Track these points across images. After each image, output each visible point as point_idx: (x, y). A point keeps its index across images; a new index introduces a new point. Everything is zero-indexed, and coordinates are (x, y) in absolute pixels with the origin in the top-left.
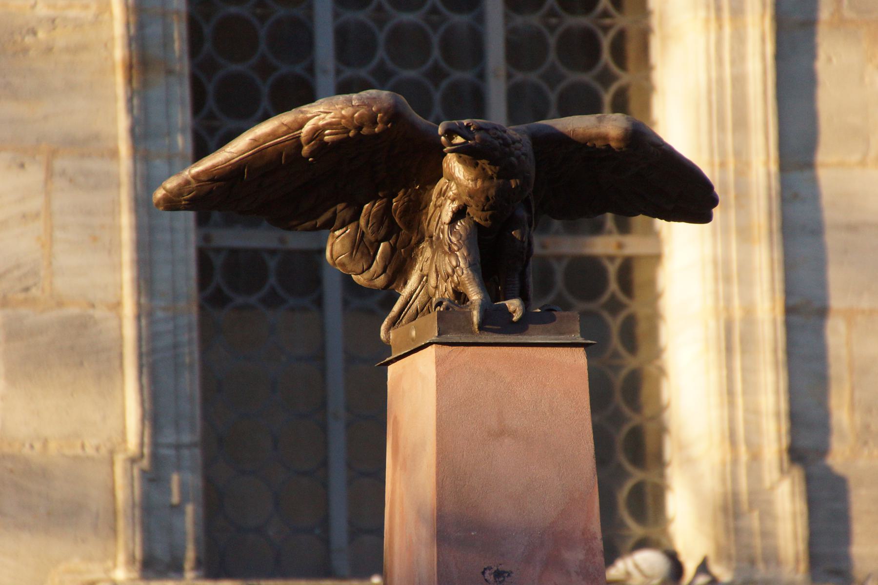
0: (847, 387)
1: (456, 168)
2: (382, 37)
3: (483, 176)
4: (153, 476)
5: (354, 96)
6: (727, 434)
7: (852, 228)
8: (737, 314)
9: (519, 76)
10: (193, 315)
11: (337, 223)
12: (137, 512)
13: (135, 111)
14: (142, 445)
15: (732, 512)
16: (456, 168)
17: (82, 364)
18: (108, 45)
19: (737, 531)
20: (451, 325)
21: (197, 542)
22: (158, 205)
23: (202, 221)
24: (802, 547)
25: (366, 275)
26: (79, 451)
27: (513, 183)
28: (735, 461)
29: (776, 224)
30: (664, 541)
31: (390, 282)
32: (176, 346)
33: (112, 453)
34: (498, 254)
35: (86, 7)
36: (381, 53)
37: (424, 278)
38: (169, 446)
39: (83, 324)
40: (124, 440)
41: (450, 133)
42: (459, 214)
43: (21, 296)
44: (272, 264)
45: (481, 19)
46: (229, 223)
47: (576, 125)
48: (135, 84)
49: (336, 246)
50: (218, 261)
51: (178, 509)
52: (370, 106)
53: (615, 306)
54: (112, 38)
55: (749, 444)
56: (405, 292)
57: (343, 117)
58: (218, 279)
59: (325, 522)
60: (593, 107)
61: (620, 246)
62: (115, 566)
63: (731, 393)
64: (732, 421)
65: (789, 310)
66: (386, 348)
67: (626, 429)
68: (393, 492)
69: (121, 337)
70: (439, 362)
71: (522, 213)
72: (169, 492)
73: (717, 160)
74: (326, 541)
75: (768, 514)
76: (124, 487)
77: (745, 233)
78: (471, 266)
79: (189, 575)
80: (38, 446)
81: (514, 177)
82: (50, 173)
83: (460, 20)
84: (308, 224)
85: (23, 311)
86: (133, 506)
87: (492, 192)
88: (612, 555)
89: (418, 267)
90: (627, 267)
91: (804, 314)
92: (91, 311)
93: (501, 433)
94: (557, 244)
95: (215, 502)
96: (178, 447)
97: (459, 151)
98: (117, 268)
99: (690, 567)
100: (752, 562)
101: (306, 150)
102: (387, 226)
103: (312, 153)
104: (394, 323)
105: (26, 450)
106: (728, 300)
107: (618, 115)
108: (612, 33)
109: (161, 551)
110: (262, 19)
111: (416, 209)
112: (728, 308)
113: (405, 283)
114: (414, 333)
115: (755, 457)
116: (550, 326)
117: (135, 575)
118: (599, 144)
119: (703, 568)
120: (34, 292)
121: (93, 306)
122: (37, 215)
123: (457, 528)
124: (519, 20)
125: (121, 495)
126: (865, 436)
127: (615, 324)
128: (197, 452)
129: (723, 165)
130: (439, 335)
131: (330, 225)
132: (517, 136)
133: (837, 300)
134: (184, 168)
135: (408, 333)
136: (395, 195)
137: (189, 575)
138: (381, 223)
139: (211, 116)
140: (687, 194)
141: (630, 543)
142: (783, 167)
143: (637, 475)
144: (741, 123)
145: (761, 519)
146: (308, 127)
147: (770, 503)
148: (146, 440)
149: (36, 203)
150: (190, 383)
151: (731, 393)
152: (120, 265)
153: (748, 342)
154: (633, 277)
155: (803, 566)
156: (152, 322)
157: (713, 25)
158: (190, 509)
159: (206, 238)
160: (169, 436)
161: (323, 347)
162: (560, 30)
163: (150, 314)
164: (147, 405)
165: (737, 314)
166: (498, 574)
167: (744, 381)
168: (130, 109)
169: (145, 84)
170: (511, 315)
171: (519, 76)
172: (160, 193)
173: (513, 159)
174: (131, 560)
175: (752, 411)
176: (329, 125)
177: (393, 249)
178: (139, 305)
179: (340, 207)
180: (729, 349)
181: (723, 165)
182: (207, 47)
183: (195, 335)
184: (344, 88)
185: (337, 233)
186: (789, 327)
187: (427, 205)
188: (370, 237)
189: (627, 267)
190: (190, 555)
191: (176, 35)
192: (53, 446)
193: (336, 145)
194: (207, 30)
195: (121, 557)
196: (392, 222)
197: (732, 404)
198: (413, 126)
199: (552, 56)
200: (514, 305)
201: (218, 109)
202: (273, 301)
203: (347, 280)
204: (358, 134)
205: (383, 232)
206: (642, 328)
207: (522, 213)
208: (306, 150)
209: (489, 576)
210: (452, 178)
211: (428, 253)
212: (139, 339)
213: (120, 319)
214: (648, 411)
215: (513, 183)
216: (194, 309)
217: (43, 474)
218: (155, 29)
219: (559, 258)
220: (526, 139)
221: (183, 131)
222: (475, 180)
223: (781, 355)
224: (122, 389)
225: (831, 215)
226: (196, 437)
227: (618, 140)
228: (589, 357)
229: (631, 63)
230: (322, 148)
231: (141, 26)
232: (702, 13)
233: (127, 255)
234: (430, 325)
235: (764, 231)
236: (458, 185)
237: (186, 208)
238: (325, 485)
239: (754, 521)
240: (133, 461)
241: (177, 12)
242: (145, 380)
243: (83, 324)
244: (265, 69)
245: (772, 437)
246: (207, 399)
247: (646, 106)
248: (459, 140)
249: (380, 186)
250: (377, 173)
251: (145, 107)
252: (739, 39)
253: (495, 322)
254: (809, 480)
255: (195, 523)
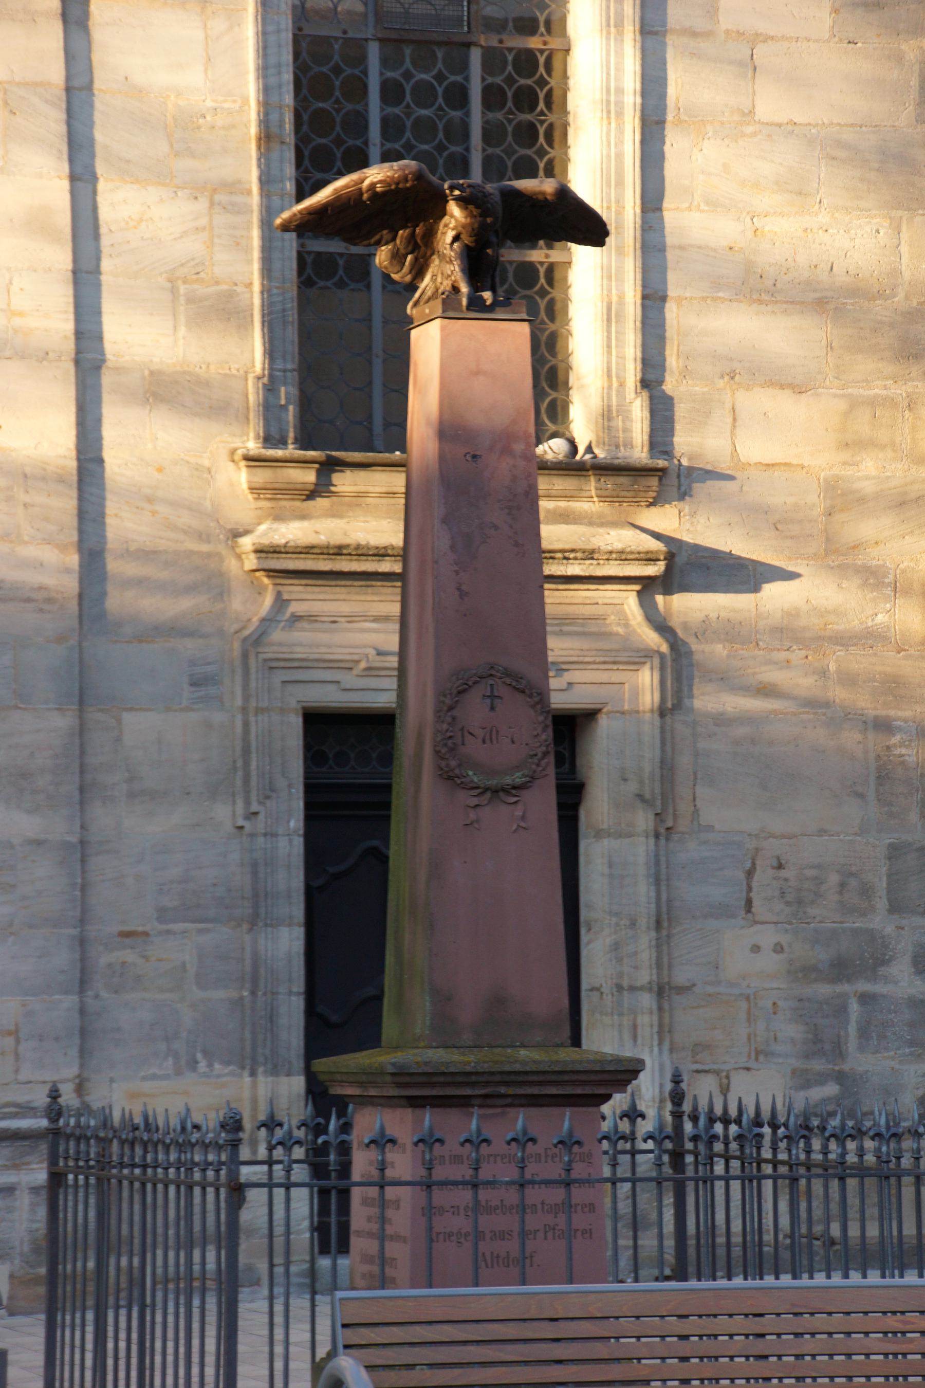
0: (676, 343)
1: (455, 210)
2: (409, 124)
3: (471, 215)
4: (270, 389)
5: (395, 164)
6: (605, 370)
7: (682, 248)
8: (614, 299)
9: (490, 150)
10: (294, 292)
11: (383, 242)
12: (261, 408)
13: (263, 166)
14: (264, 369)
15: (607, 417)
16: (455, 210)
17: (229, 319)
18: (247, 126)
19: (609, 428)
20: (449, 306)
21: (295, 427)
22: (277, 228)
23: (300, 236)
24: (646, 438)
25: (400, 274)
26: (228, 372)
27: (489, 220)
28: (610, 387)
29: (638, 245)
30: (567, 433)
31: (414, 279)
32: (284, 310)
33: (246, 373)
34: (479, 264)
35: (235, 101)
36: (408, 134)
37: (434, 276)
38: (279, 370)
39: (230, 295)
40: (254, 366)
41: (452, 188)
42: (456, 238)
43: (195, 277)
44: (341, 262)
45: (468, 114)
46: (316, 237)
47: (526, 185)
48: (262, 150)
49: (382, 256)
50: (309, 259)
51: (284, 408)
52: (404, 170)
53: (543, 293)
54: (249, 121)
55: (618, 377)
56: (423, 285)
57: (388, 177)
58: (309, 270)
59: (370, 418)
60: (533, 175)
61: (547, 256)
62: (248, 440)
63: (609, 346)
64: (609, 363)
65: (644, 297)
66: (410, 320)
67: (547, 367)
68: (413, 406)
69: (252, 304)
70: (443, 329)
71: (494, 239)
72: (279, 398)
73: (605, 205)
74: (370, 430)
75: (627, 418)
76: (253, 395)
77: (620, 251)
78: (463, 270)
79: (291, 446)
80: (204, 367)
81: (489, 216)
82: (212, 204)
83: (456, 114)
84: (366, 242)
85: (196, 286)
86: (259, 406)
87: (476, 226)
88: (539, 442)
89: (430, 270)
90: (551, 269)
91: (653, 299)
92: (235, 288)
93: (478, 373)
94: (512, 255)
95: (305, 404)
96: (285, 371)
97: (457, 199)
98: (250, 262)
99: (581, 449)
100: (617, 446)
101: (365, 196)
102: (413, 245)
103: (369, 199)
104: (416, 304)
105: (197, 369)
106: (610, 290)
107: (551, 180)
108: (545, 125)
109: (274, 433)
110: (338, 111)
111: (430, 235)
112: (609, 296)
113: (423, 280)
114: (427, 311)
115: (622, 385)
116: (508, 308)
117: (260, 445)
118: (541, 197)
119: (589, 449)
120: (202, 275)
121: (236, 285)
122: (204, 228)
123: (450, 431)
124: (490, 115)
125: (252, 398)
126: (685, 373)
127: (542, 304)
128: (296, 374)
129: (609, 208)
130: (443, 312)
131: (378, 243)
132: (491, 191)
133: (672, 292)
134: (291, 206)
135: (424, 311)
136: (417, 226)
137: (291, 446)
138: (409, 242)
139: (307, 171)
140: (590, 229)
141: (547, 434)
142: (644, 211)
143: (554, 395)
144: (620, 183)
145: (623, 421)
146: (366, 183)
147: (629, 411)
148: (266, 366)
149: (204, 221)
150: (292, 333)
151: (609, 346)
152: (252, 260)
153: (620, 317)
154: (554, 275)
155: (646, 449)
156: (270, 295)
157: (605, 122)
158: (291, 408)
159: (302, 245)
160: (279, 365)
161: (370, 314)
162: (514, 122)
163: (269, 291)
164: (267, 345)
165: (614, 299)
166: (474, 457)
167: (617, 339)
168: (259, 166)
169: (268, 149)
170: (485, 301)
171: (490, 150)
172: (278, 221)
173: (489, 205)
174: (257, 437)
175: (622, 358)
176: (380, 182)
177: (416, 259)
178: (263, 285)
179: (385, 232)
180: (609, 320)
181: (609, 208)
182: (305, 128)
183: (295, 304)
184: (387, 157)
185: (383, 248)
186: (644, 307)
187: (437, 232)
188: (402, 251)
189: (551, 269)
190: (291, 435)
191: (287, 120)
192: (212, 367)
193: (384, 194)
194: (305, 117)
195: (252, 435)
196: (416, 243)
197: (609, 353)
198: (429, 183)
199: (510, 138)
200: (487, 295)
201: (312, 168)
202: (341, 285)
203: (387, 277)
204: (397, 188)
205: (410, 248)
206: (558, 306)
207: (494, 239)
208: (365, 196)
209: (468, 457)
210: (452, 216)
211: (437, 262)
212: (263, 305)
213: (252, 293)
214: (560, 357)
215: (489, 220)
216: (295, 288)
217: (207, 384)
218: (274, 117)
219: (511, 262)
220: (497, 193)
221: (290, 179)
222: (466, 218)
223: (639, 324)
224: (253, 337)
225: (670, 240)
226: (295, 366)
227: (551, 195)
228: (531, 325)
229: (556, 144)
230: (375, 196)
231: (266, 114)
232: (599, 114)
233: (256, 254)
234: (438, 305)
235: (631, 249)
236: (456, 220)
237: (293, 231)
238: (370, 397)
239: (619, 423)
240: (259, 378)
241: (288, 106)
242: (266, 331)
243: (230, 295)
244: (339, 142)
245: (632, 373)
246: (301, 344)
247: (565, 171)
248: (457, 192)
249: (410, 220)
250: (408, 210)
251: (268, 165)
252: (620, 130)
253: (476, 304)
254: (651, 398)
255: (294, 416)
